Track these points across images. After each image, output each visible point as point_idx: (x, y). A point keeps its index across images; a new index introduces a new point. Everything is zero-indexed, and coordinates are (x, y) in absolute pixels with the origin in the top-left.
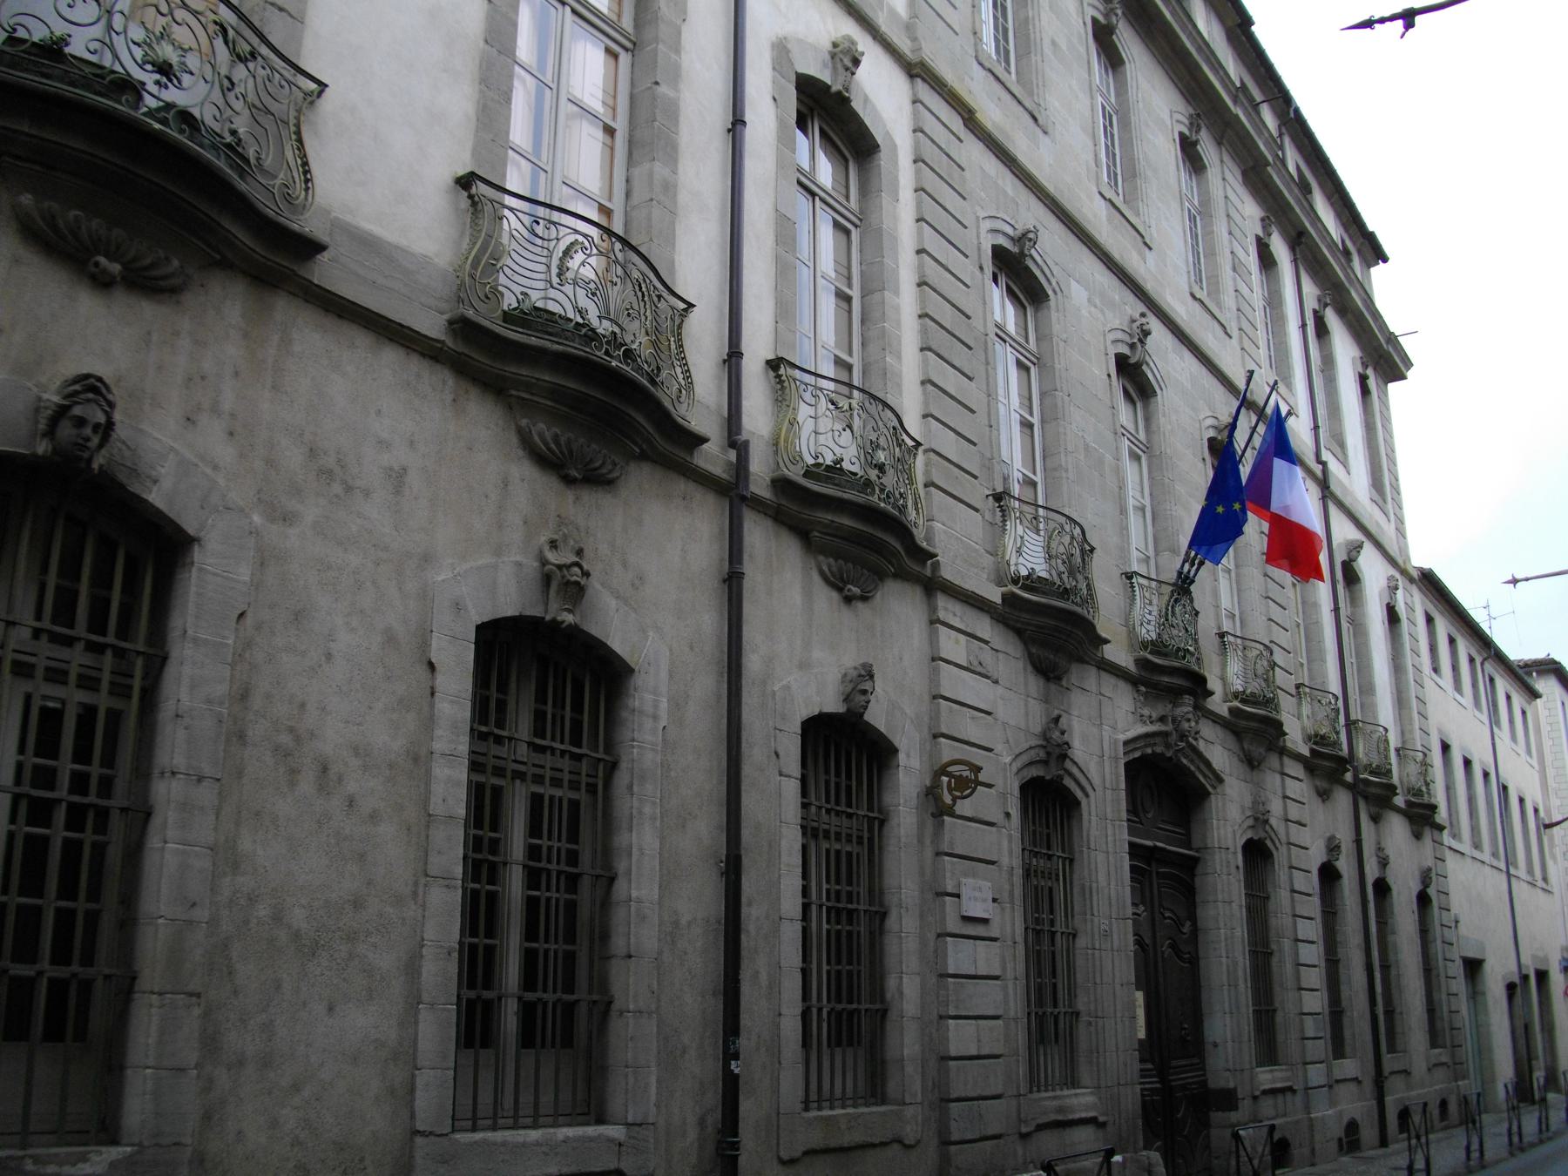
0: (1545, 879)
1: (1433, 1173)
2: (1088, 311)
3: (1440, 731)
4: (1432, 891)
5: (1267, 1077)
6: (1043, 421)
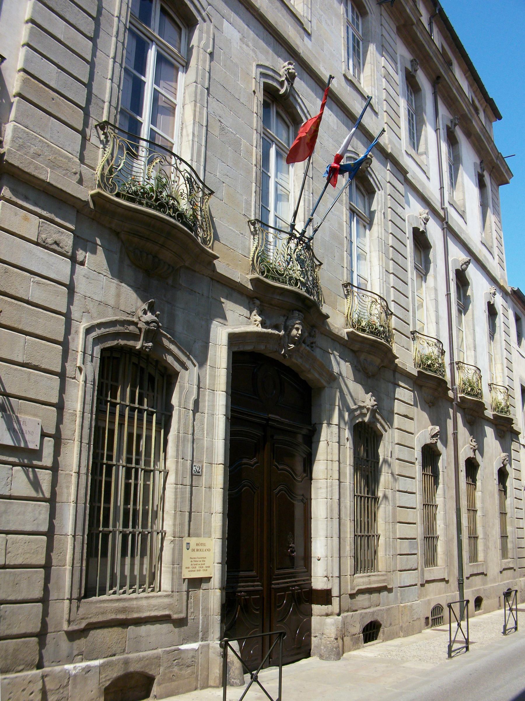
2: (445, 256)
3: (521, 380)
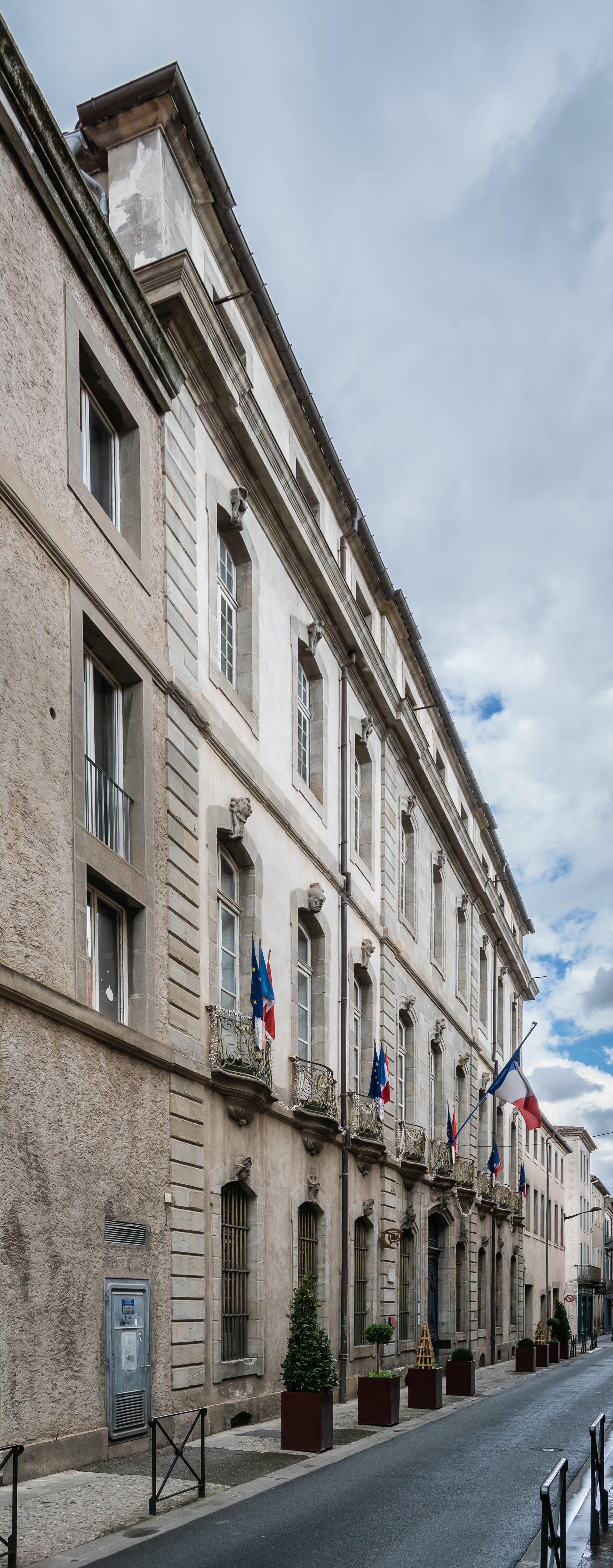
0: (562, 1245)
1: (19, 1562)
4: (516, 1256)
5: (460, 1336)
6: (406, 1080)
